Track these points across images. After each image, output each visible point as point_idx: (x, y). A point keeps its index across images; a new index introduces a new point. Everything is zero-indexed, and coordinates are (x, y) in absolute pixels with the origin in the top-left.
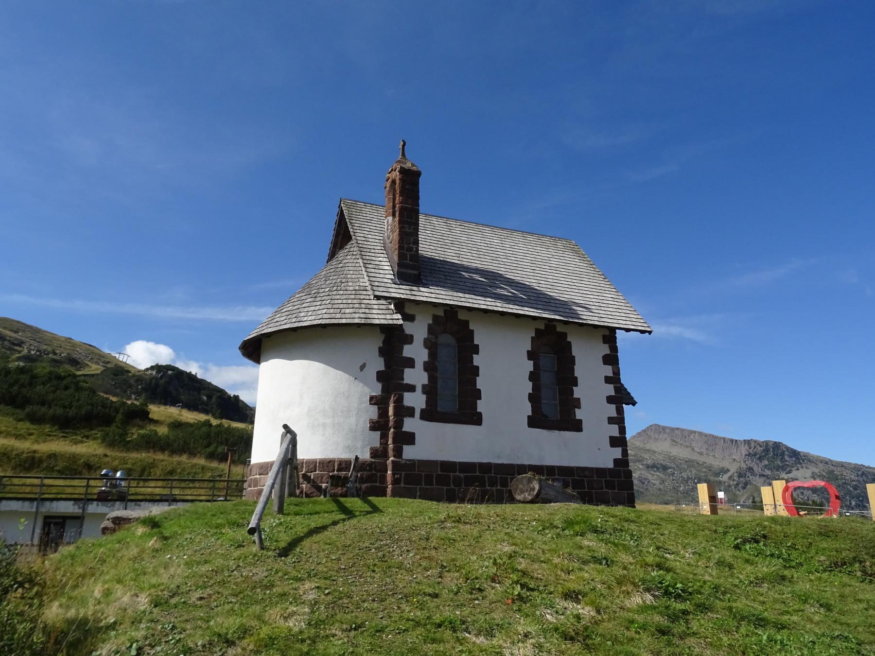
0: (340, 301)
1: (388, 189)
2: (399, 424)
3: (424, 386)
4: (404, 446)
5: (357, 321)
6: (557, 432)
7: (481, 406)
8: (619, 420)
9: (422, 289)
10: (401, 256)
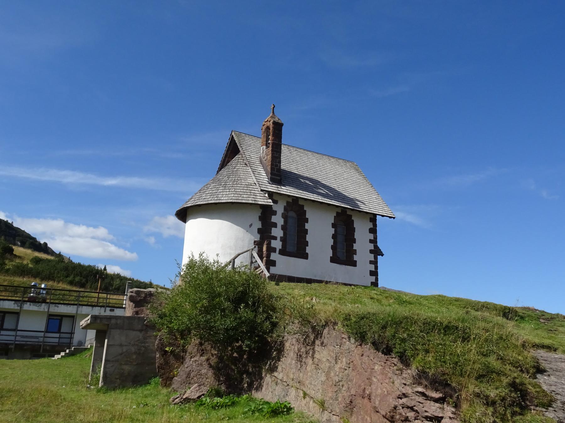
0: (239, 190)
1: (263, 130)
2: (268, 256)
3: (281, 237)
4: (271, 267)
5: (250, 202)
6: (344, 266)
7: (308, 250)
8: (375, 263)
9: (282, 187)
10: (272, 169)
